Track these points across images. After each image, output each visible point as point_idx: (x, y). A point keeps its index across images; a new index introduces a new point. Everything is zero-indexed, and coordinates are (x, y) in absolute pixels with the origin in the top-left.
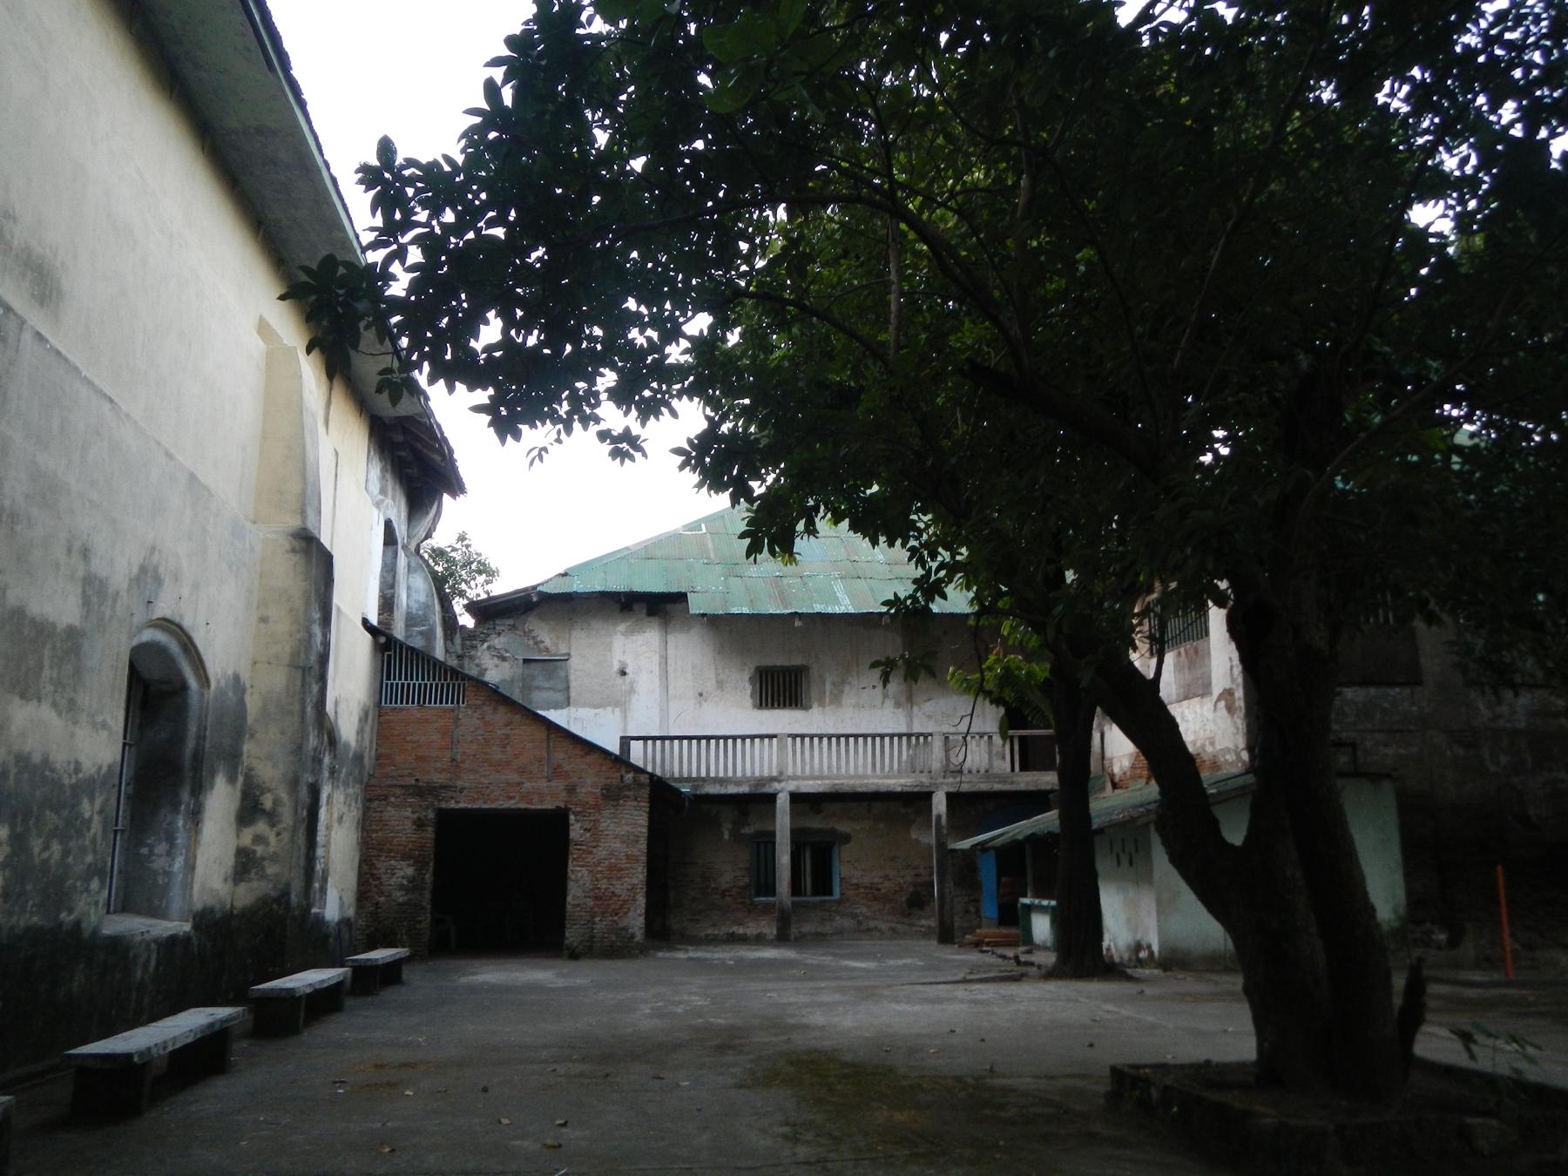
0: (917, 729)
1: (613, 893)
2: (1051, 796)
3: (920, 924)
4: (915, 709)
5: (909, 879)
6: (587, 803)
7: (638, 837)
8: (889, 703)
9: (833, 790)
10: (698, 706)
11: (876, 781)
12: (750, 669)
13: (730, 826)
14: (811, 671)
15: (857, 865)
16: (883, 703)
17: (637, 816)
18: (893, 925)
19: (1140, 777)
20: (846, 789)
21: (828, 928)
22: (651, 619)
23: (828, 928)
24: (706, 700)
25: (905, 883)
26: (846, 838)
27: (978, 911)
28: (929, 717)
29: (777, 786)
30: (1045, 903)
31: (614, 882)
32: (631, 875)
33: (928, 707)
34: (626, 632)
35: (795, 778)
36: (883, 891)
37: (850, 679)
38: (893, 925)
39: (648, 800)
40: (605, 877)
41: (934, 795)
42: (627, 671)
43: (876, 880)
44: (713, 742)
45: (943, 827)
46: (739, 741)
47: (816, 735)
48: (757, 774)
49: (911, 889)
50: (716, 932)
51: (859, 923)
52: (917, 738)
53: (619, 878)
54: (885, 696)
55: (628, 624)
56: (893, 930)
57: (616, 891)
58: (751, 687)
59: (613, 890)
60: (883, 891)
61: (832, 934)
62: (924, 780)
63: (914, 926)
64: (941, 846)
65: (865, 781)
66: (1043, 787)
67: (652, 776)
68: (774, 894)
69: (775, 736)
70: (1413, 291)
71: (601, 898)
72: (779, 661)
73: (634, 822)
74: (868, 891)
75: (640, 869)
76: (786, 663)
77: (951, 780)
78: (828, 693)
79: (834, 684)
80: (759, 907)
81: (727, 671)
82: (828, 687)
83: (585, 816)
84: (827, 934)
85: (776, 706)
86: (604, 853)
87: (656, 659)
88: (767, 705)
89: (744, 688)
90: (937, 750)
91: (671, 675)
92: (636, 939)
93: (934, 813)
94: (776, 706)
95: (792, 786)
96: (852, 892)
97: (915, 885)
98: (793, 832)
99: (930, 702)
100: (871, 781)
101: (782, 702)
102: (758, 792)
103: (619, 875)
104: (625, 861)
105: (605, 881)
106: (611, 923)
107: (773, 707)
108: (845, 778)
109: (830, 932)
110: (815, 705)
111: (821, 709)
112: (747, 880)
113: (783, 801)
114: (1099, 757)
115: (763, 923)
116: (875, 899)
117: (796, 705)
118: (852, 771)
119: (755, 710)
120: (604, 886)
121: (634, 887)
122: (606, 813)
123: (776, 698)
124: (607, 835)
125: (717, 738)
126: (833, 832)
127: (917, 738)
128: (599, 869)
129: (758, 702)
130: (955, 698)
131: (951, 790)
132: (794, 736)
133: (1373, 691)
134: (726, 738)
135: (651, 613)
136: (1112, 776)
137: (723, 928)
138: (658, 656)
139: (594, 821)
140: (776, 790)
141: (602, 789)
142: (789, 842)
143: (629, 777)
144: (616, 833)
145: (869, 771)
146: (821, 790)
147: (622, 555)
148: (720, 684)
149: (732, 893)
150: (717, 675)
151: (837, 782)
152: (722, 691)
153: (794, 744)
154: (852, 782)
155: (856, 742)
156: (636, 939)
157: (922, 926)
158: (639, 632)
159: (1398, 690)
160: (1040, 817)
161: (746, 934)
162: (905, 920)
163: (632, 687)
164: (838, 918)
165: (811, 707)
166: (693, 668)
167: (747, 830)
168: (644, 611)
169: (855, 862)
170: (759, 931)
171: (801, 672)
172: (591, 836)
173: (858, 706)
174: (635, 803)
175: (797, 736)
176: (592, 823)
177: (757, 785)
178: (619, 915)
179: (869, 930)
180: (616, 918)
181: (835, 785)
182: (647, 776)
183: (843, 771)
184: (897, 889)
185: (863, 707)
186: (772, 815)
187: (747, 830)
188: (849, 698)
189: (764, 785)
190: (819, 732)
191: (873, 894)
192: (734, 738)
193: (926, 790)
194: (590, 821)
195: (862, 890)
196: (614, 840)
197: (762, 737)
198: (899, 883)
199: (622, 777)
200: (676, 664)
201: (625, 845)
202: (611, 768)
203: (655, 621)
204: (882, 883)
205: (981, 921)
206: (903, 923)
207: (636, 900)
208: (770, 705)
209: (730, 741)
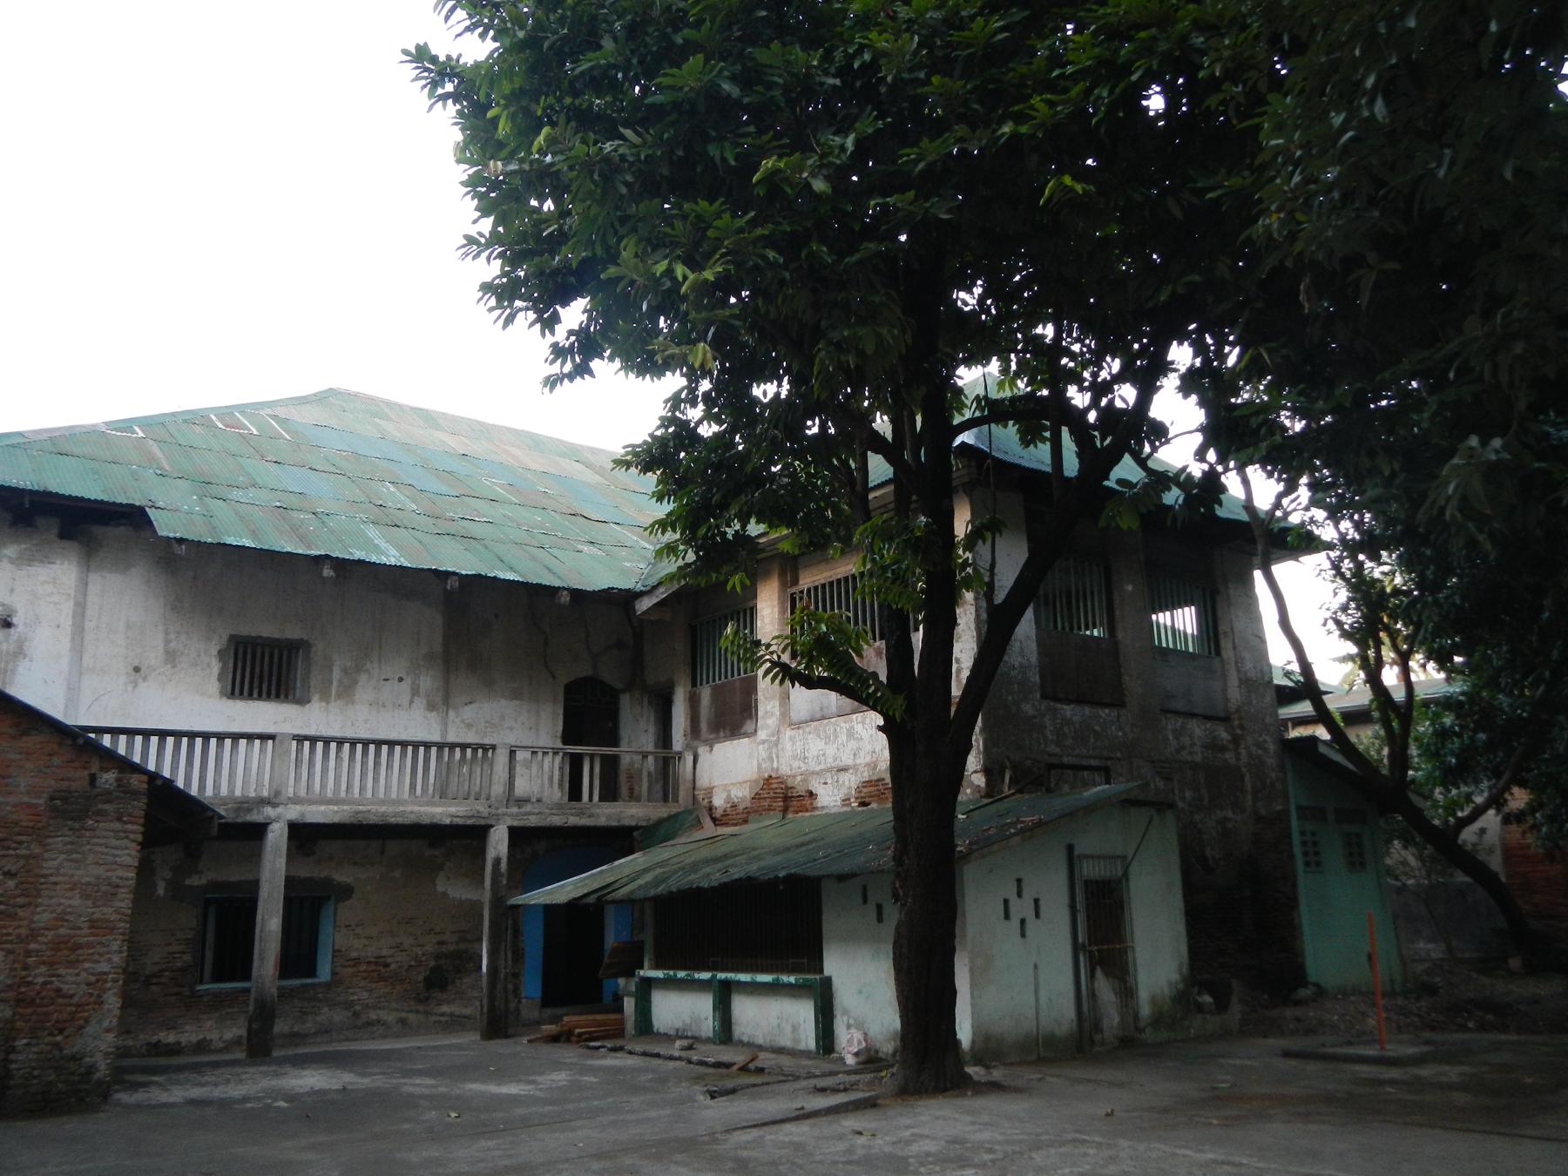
0: (452, 738)
1: (58, 990)
2: (635, 834)
3: (440, 1011)
4: (452, 713)
5: (429, 948)
6: (16, 823)
7: (118, 886)
8: (420, 703)
9: (354, 821)
10: (130, 688)
11: (416, 808)
12: (221, 637)
13: (168, 874)
14: (313, 649)
15: (359, 930)
16: (411, 702)
17: (116, 848)
18: (404, 1015)
19: (770, 809)
20: (373, 819)
21: (309, 1026)
22: (66, 544)
23: (309, 1026)
24: (145, 679)
25: (423, 955)
26: (345, 892)
27: (516, 990)
28: (469, 726)
29: (269, 811)
30: (705, 975)
31: (62, 971)
32: (97, 957)
33: (468, 712)
34: (19, 558)
35: (296, 800)
36: (393, 966)
37: (368, 666)
38: (404, 1015)
39: (142, 821)
40: (44, 963)
41: (493, 829)
42: (15, 620)
43: (385, 952)
44: (170, 740)
45: (501, 875)
46: (213, 741)
47: (333, 739)
48: (238, 793)
49: (432, 963)
50: (130, 1043)
51: (356, 1014)
52: (475, 750)
53: (71, 964)
54: (415, 692)
55: (23, 546)
56: (403, 1021)
57: (65, 987)
58: (220, 664)
59: (57, 984)
60: (393, 966)
61: (314, 1033)
62: (481, 809)
63: (432, 1014)
64: (497, 901)
65: (402, 809)
66: (627, 822)
67: (154, 777)
68: (246, 975)
69: (272, 737)
70: (1155, 256)
71: (33, 1001)
72: (266, 630)
73: (110, 859)
74: (373, 967)
75: (115, 946)
76: (277, 635)
77: (515, 810)
78: (335, 683)
79: (345, 670)
80: (205, 999)
81: (183, 637)
82: (336, 674)
83: (9, 848)
84: (306, 1035)
85: (255, 695)
86: (46, 916)
87: (68, 607)
88: (241, 693)
89: (209, 665)
90: (501, 768)
91: (89, 637)
92: (97, 1076)
93: (491, 855)
94: (255, 695)
95: (293, 813)
96: (350, 970)
97: (437, 957)
98: (290, 882)
99: (471, 706)
100: (409, 809)
101: (273, 692)
102: (239, 820)
103: (73, 957)
104: (86, 931)
105: (43, 969)
106: (49, 1048)
107: (250, 696)
108: (373, 803)
109: (313, 1031)
110: (316, 698)
111: (324, 704)
112: (187, 958)
113: (277, 836)
114: (690, 785)
115: (209, 1023)
116: (381, 979)
117: (286, 697)
118: (381, 795)
119: (224, 699)
120: (40, 980)
121: (101, 978)
122: (57, 842)
123: (256, 684)
124: (56, 883)
125: (177, 734)
126: (328, 882)
127: (475, 750)
128: (33, 946)
129: (229, 687)
130: (503, 702)
131: (516, 823)
132: (300, 739)
133: (1087, 710)
134: (192, 735)
135: (65, 535)
136: (711, 809)
137: (141, 1036)
138: (71, 603)
139: (27, 857)
140: (270, 818)
141: (52, 799)
142: (282, 897)
143: (108, 778)
144: (76, 878)
145: (406, 796)
146: (336, 819)
147: (14, 441)
148: (171, 657)
149: (163, 980)
150: (167, 642)
151: (361, 808)
152: (174, 667)
153: (299, 751)
154: (383, 809)
155: (391, 753)
156: (97, 1076)
157: (443, 1015)
158: (42, 562)
159: (1107, 711)
160: (623, 860)
161: (179, 1043)
162: (421, 1008)
163: (20, 647)
164: (326, 1010)
165: (309, 701)
166: (129, 627)
167: (195, 881)
168: (55, 531)
169: (357, 925)
170: (202, 1036)
171: (298, 650)
172: (17, 886)
173: (377, 704)
174: (117, 825)
175: (306, 738)
176: (22, 863)
177: (238, 810)
178: (66, 1033)
179: (369, 1024)
180: (59, 1038)
181: (357, 813)
182: (145, 778)
183: (369, 794)
184: (413, 963)
185: (384, 706)
186: (256, 857)
187: (195, 881)
188: (364, 692)
189: (249, 810)
190: (338, 735)
191: (378, 970)
192: (206, 736)
193: (483, 822)
194: (18, 856)
195: (363, 967)
196: (69, 894)
197: (250, 737)
198: (417, 955)
199: (93, 778)
200: (100, 618)
201: (89, 903)
202: (72, 761)
203: (72, 548)
204: (391, 956)
205: (520, 1002)
206: (417, 1012)
207: (102, 1003)
208: (246, 693)
209: (199, 741)
